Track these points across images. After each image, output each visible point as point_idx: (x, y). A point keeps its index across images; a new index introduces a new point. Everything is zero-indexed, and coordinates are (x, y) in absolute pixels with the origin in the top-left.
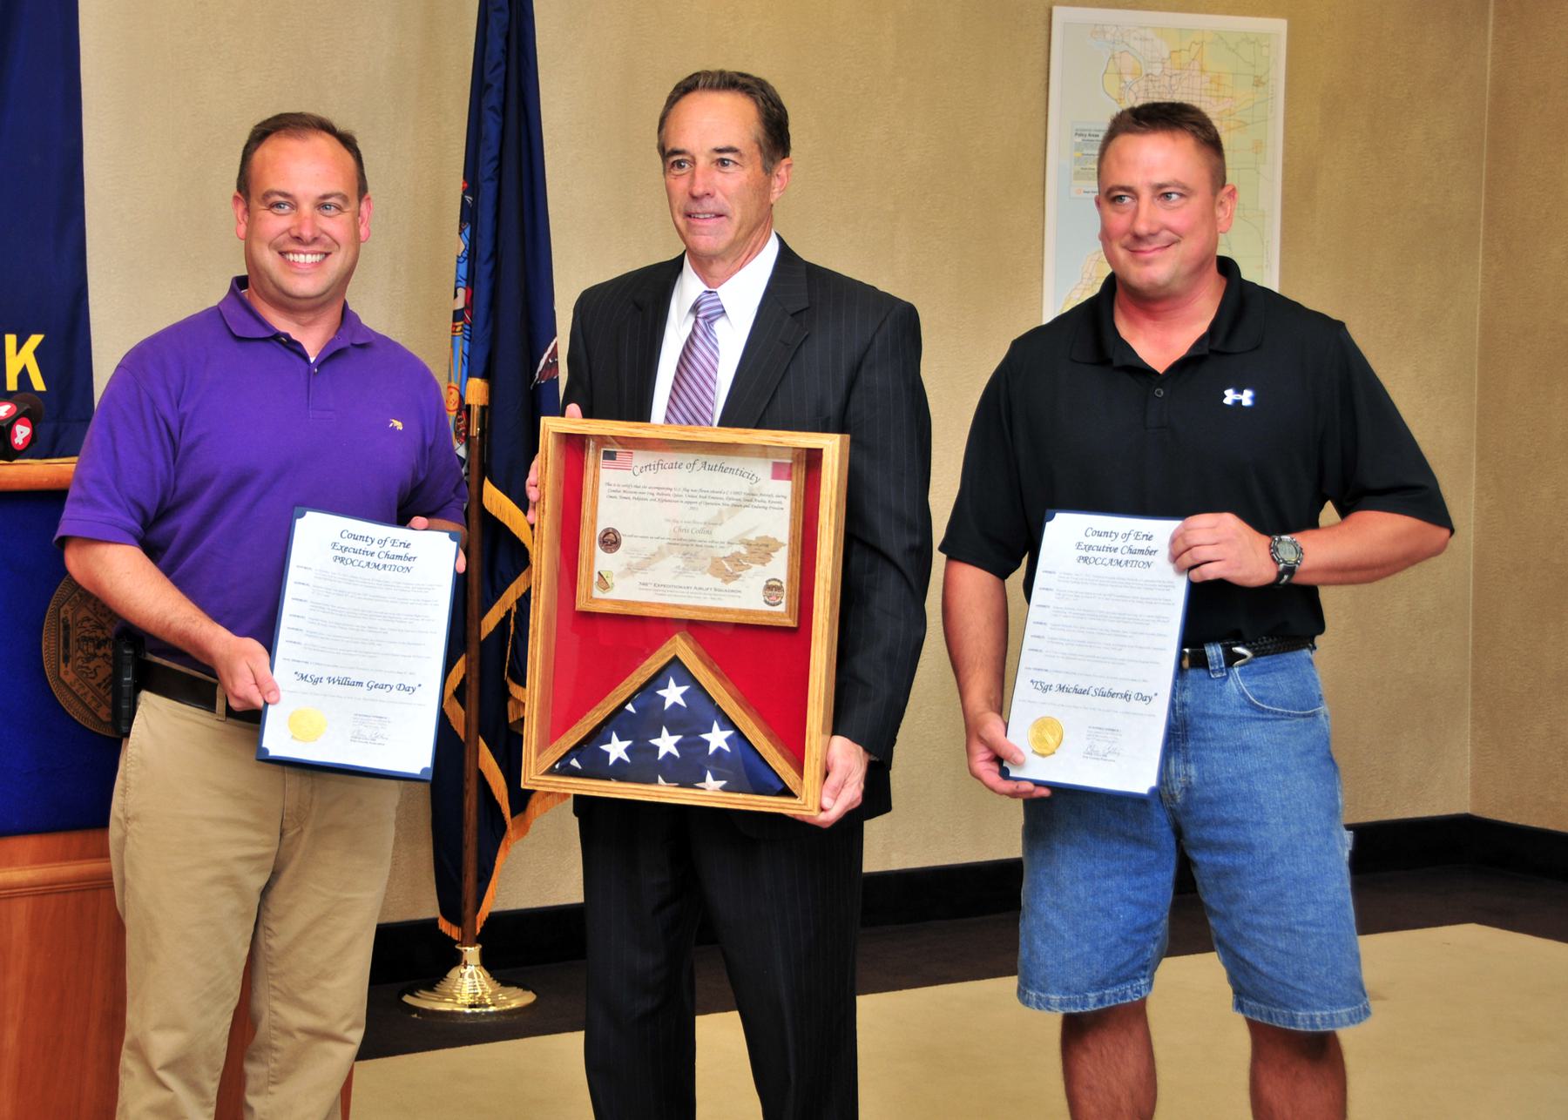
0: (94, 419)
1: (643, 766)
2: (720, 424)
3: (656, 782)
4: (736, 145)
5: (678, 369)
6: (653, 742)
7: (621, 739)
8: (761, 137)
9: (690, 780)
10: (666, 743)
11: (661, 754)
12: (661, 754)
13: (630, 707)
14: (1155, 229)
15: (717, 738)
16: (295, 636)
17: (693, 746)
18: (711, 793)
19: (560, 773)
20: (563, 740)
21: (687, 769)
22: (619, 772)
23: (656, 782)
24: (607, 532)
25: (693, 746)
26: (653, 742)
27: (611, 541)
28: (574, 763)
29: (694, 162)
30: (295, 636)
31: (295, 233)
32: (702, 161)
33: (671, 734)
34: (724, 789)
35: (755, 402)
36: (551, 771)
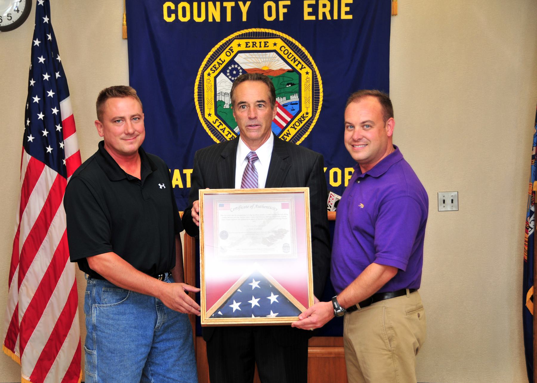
0: (69, 254)
1: (246, 311)
2: (269, 184)
3: (251, 317)
4: (264, 99)
5: (243, 179)
6: (249, 302)
7: (270, 296)
8: (271, 96)
9: (264, 315)
10: (254, 302)
11: (253, 306)
12: (253, 306)
13: (239, 290)
14: (360, 137)
15: (273, 298)
16: (276, 59)
17: (264, 301)
18: (272, 319)
19: (214, 317)
20: (286, 291)
21: (262, 311)
22: (238, 314)
23: (251, 317)
24: (223, 232)
25: (264, 301)
26: (249, 302)
27: (224, 235)
28: (220, 313)
29: (249, 106)
30: (276, 59)
31: (126, 132)
32: (252, 106)
33: (237, 302)
34: (277, 316)
35: (278, 178)
36: (211, 317)
